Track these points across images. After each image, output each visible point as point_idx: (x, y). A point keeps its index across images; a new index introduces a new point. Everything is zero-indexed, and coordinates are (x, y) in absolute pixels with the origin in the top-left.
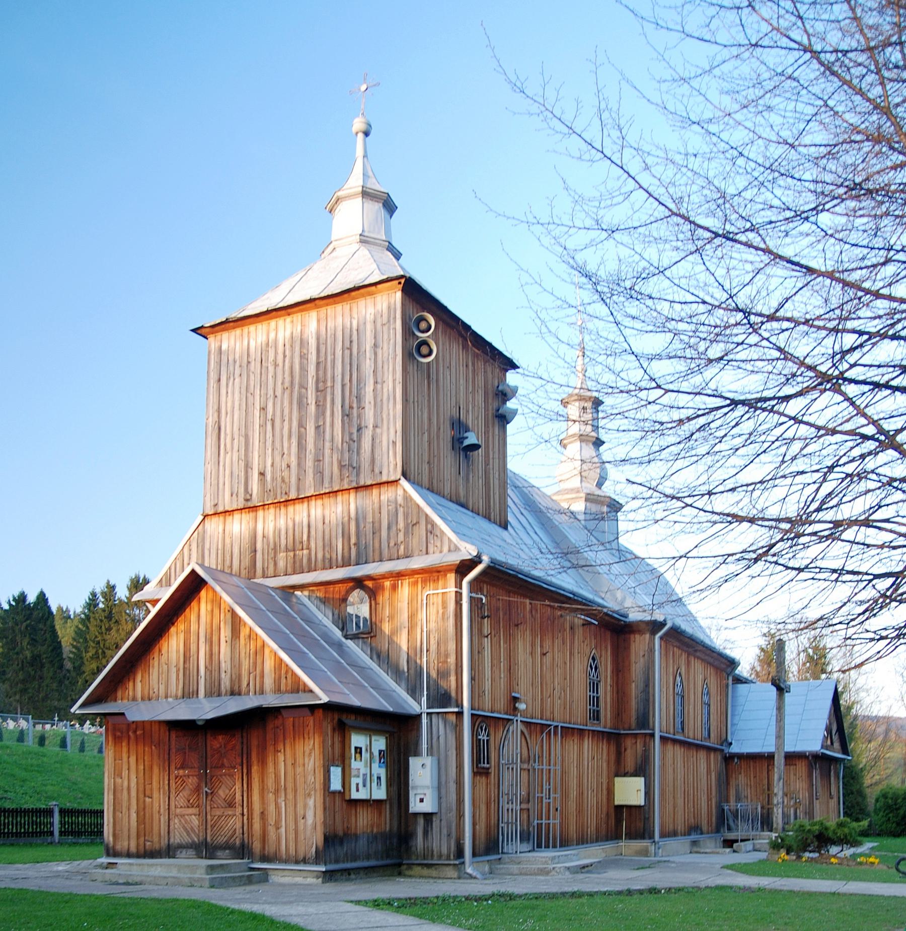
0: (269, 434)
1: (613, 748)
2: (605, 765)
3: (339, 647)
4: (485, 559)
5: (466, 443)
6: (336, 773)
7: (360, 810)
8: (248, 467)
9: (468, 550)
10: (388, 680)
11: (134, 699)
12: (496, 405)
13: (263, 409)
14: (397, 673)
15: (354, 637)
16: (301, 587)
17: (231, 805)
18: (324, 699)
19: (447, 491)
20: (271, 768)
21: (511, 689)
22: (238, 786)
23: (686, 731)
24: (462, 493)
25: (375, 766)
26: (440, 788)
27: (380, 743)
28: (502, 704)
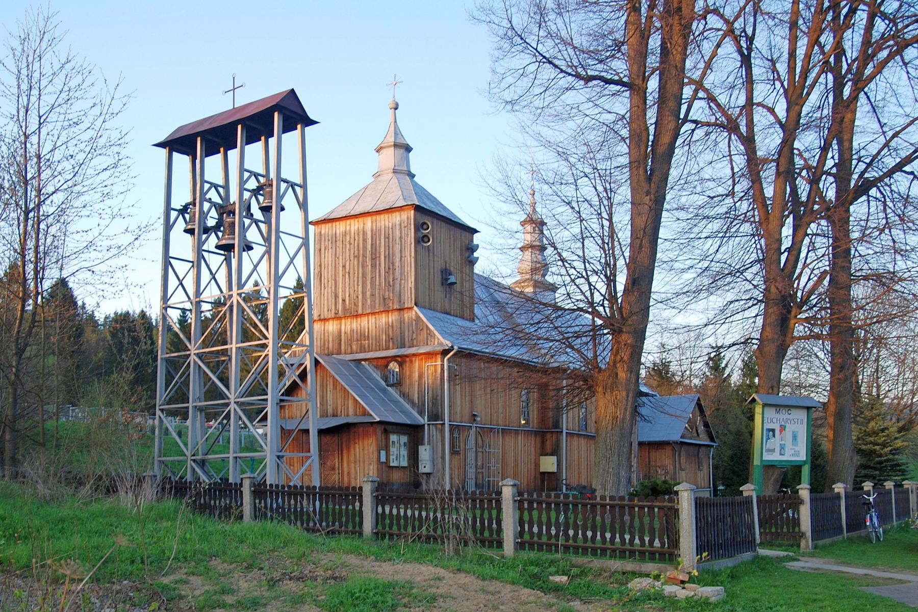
0: (347, 280)
1: (539, 440)
2: (533, 449)
3: (384, 391)
4: (456, 348)
5: (449, 282)
6: (383, 453)
7: (394, 471)
8: (336, 296)
9: (447, 343)
10: (408, 407)
11: (677, 569)
12: (467, 254)
13: (344, 266)
14: (413, 404)
15: (392, 386)
16: (365, 360)
17: (333, 469)
18: (378, 419)
19: (439, 308)
20: (352, 452)
21: (472, 409)
22: (337, 460)
23: (589, 429)
24: (447, 306)
25: (402, 449)
26: (433, 461)
27: (404, 439)
28: (467, 417)
